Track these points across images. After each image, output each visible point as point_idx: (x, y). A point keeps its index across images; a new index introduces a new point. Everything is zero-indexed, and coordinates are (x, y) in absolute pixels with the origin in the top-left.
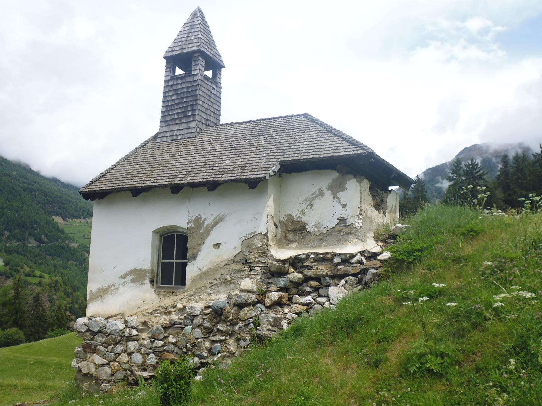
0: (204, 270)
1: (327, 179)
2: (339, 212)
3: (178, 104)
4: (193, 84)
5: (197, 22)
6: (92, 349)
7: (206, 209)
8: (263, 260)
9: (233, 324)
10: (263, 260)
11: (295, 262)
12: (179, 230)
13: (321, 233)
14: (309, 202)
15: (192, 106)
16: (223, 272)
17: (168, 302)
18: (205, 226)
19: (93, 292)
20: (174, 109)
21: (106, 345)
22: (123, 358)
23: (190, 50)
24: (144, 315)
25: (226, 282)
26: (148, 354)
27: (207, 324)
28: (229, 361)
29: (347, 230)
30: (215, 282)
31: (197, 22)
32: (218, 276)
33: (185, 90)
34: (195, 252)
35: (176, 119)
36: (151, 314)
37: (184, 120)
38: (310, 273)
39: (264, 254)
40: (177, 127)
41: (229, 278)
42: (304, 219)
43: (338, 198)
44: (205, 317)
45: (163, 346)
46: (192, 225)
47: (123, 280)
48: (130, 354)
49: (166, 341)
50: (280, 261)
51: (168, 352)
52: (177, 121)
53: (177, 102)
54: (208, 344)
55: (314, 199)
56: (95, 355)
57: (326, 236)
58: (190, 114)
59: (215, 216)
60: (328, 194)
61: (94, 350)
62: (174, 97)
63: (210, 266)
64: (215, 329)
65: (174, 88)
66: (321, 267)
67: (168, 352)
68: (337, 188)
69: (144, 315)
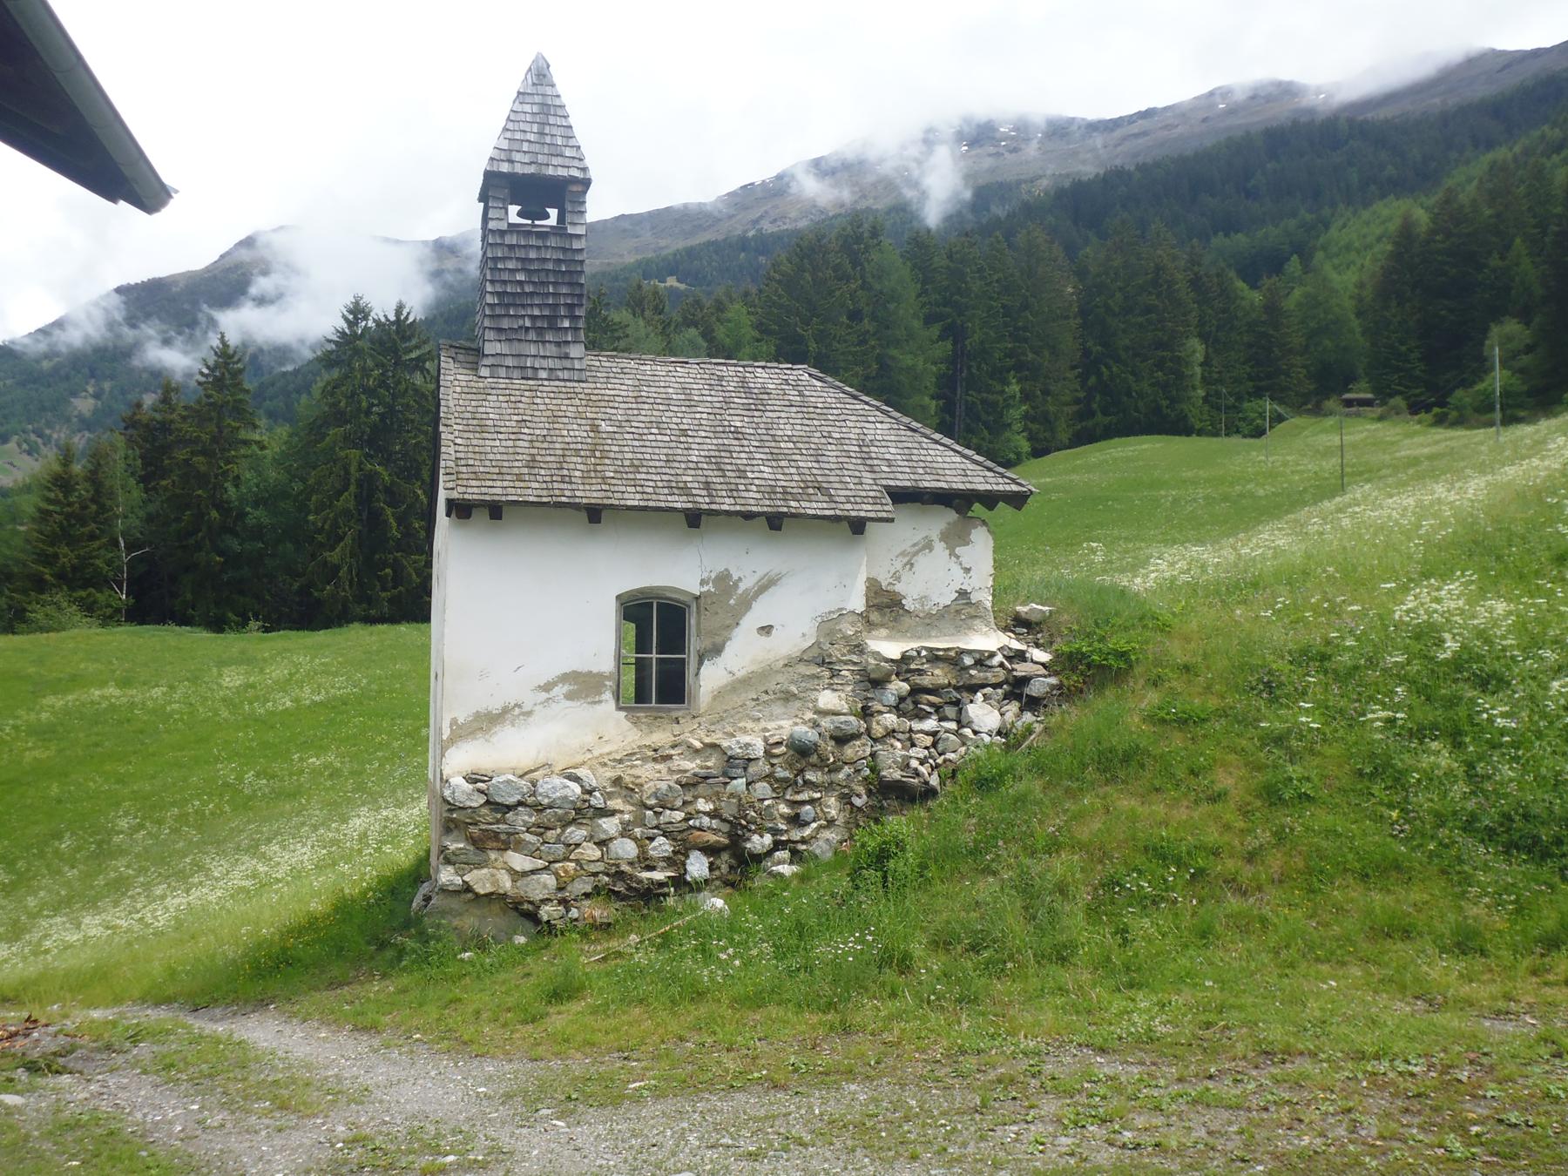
0: (739, 675)
1: (938, 521)
2: (958, 580)
3: (532, 294)
4: (569, 256)
5: (539, 102)
6: (503, 842)
7: (745, 561)
8: (855, 658)
9: (834, 769)
10: (855, 658)
11: (903, 665)
12: (669, 595)
13: (929, 615)
14: (906, 560)
15: (571, 306)
16: (780, 678)
17: (661, 737)
18: (740, 591)
19: (461, 720)
20: (523, 306)
21: (541, 829)
22: (589, 852)
23: (562, 172)
24: (605, 765)
25: (788, 697)
26: (652, 839)
27: (781, 773)
28: (827, 834)
29: (971, 610)
30: (766, 698)
31: (539, 102)
32: (772, 686)
33: (550, 266)
34: (718, 640)
35: (527, 329)
36: (620, 761)
37: (549, 337)
38: (926, 681)
39: (859, 649)
40: (533, 350)
41: (794, 689)
42: (899, 588)
43: (958, 557)
44: (774, 761)
45: (686, 820)
46: (710, 587)
47: (544, 695)
48: (602, 844)
49: (690, 809)
50: (892, 661)
51: (700, 829)
52: (532, 336)
53: (528, 289)
54: (784, 809)
55: (916, 554)
56: (510, 853)
57: (934, 620)
58: (566, 324)
59: (760, 574)
60: (940, 547)
61: (507, 843)
62: (520, 277)
63: (754, 668)
64: (800, 781)
65: (521, 254)
66: (937, 672)
67: (700, 829)
68: (955, 538)
69: (605, 765)
